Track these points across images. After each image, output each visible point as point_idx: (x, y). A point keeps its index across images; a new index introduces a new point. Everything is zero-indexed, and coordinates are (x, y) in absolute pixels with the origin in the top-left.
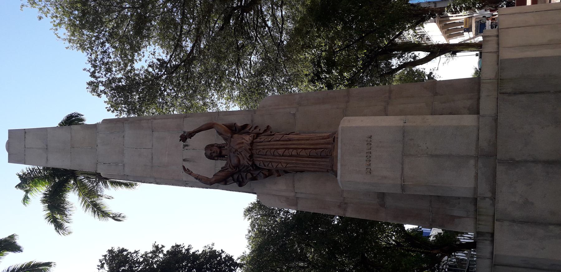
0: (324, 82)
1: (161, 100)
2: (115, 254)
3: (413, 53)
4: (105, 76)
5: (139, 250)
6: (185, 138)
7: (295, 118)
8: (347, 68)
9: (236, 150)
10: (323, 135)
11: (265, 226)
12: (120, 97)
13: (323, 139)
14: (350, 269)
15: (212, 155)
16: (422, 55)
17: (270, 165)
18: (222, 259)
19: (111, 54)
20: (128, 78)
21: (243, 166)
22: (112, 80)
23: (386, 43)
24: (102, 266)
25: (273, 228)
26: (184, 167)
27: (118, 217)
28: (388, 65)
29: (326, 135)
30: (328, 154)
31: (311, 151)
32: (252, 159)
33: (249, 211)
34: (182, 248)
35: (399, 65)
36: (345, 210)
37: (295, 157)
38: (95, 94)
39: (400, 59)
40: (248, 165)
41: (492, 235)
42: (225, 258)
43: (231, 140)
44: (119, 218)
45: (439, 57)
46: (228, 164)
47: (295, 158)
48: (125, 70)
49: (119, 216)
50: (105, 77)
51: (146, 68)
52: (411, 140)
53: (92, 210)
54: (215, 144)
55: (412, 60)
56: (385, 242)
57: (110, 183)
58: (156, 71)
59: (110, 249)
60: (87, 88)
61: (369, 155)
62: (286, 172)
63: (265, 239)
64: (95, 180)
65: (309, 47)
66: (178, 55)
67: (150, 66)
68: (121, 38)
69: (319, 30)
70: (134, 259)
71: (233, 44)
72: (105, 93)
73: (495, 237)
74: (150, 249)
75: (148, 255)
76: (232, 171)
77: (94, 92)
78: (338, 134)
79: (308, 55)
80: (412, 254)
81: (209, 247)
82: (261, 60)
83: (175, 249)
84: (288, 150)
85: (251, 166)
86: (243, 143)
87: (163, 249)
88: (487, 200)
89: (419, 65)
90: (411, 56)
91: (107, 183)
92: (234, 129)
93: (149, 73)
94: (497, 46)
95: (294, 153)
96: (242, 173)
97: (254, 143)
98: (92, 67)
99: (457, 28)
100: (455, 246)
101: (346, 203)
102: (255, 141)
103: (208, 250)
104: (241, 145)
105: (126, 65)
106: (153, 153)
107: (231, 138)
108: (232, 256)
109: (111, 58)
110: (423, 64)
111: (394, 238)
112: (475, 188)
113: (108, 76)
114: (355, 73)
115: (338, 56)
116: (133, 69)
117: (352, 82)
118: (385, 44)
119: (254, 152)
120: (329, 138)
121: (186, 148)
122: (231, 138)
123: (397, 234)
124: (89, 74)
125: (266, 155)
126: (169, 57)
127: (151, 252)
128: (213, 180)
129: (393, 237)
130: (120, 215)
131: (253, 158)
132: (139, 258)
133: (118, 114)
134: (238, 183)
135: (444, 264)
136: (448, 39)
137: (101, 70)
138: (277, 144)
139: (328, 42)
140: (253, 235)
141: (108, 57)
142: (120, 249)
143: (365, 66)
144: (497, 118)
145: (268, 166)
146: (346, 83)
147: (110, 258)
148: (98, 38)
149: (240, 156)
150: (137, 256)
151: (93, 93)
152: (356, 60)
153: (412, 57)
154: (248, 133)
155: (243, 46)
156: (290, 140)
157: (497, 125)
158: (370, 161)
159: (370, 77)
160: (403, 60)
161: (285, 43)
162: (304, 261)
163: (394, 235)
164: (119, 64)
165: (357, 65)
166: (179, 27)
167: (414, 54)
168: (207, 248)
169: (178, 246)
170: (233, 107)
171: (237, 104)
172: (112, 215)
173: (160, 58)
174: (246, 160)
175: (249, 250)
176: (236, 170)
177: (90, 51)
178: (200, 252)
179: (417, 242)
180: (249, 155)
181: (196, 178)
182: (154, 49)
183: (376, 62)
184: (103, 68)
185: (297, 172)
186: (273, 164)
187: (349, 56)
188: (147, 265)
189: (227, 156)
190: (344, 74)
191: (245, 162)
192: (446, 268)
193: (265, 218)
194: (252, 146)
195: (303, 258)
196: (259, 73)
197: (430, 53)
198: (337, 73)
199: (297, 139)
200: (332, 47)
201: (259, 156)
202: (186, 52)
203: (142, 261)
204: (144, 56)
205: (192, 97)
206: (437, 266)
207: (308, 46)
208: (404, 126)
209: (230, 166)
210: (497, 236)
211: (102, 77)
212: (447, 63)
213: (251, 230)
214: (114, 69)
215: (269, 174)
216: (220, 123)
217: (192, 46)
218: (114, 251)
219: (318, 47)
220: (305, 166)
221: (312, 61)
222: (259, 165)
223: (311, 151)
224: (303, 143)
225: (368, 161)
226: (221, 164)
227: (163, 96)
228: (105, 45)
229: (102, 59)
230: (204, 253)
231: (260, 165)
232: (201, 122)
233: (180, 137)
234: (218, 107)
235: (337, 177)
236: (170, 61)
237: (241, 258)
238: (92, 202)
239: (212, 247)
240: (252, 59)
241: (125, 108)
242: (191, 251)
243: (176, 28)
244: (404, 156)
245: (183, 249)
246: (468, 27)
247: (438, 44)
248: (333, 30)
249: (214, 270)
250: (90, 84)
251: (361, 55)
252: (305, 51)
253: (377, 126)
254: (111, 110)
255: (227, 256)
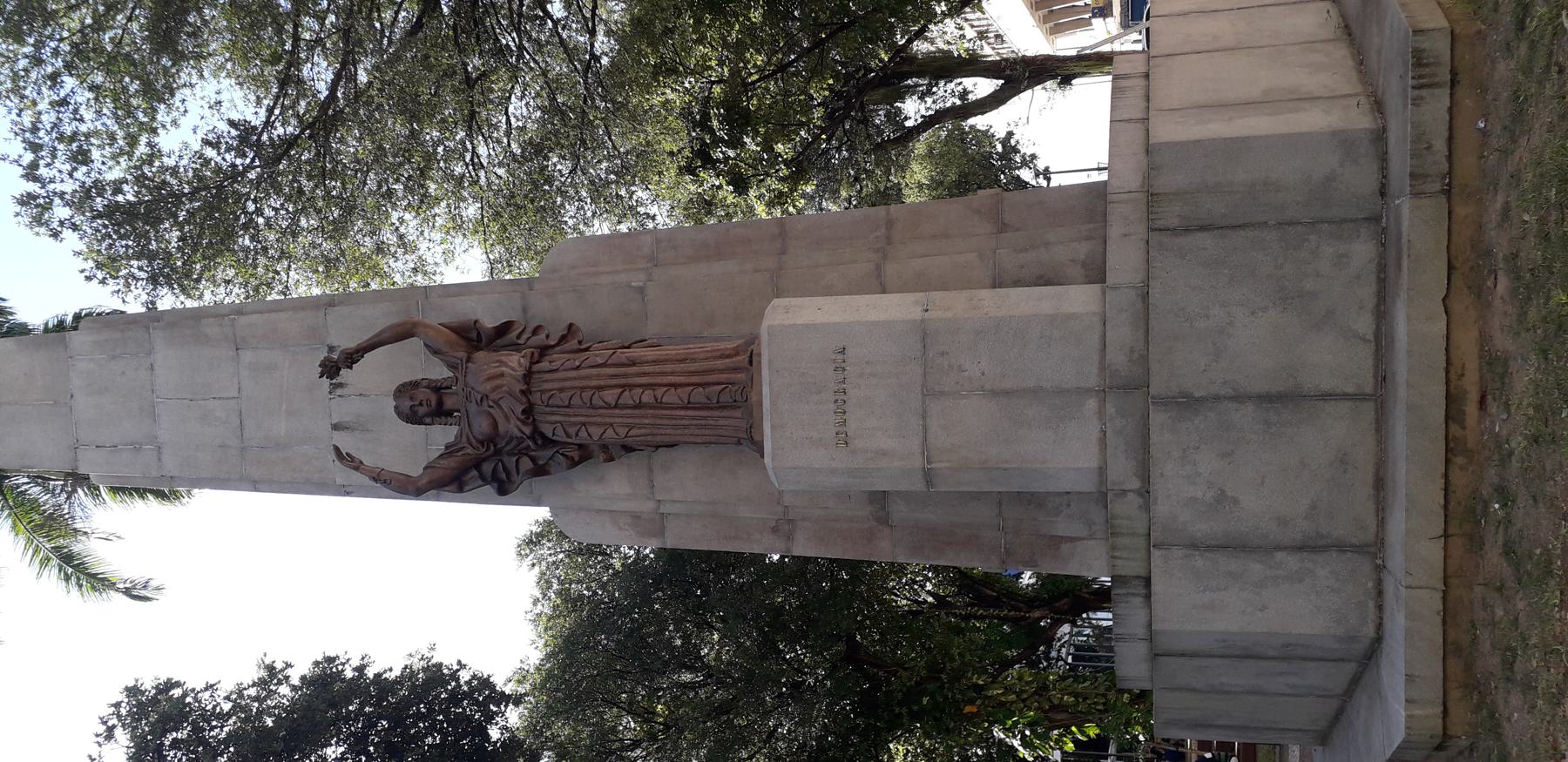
0: (722, 170)
1: (247, 242)
2: (147, 696)
3: (960, 83)
4: (71, 175)
5: (219, 682)
6: (334, 368)
7: (643, 300)
8: (784, 129)
9: (485, 397)
10: (723, 347)
11: (579, 582)
12: (121, 237)
13: (723, 356)
14: (816, 680)
15: (415, 413)
16: (982, 87)
17: (583, 434)
18: (461, 686)
19: (82, 111)
20: (140, 180)
21: (506, 440)
22: (91, 187)
23: (886, 59)
24: (110, 734)
25: (603, 586)
26: (337, 449)
27: (140, 589)
28: (895, 117)
29: (730, 345)
30: (738, 398)
31: (693, 390)
32: (532, 418)
33: (532, 542)
34: (343, 664)
35: (922, 116)
36: (790, 537)
37: (651, 408)
38: (43, 230)
39: (927, 99)
40: (522, 435)
41: (1147, 581)
42: (468, 683)
43: (466, 368)
44: (143, 593)
45: (1030, 91)
46: (464, 436)
47: (651, 411)
48: (130, 155)
49: (145, 587)
50: (71, 181)
51: (196, 146)
52: (942, 354)
53: (60, 571)
54: (423, 379)
55: (958, 102)
56: (908, 599)
57: (109, 490)
58: (227, 156)
59: (131, 684)
60: (17, 214)
61: (842, 398)
62: (628, 449)
63: (582, 620)
64: (62, 483)
65: (674, 71)
66: (293, 107)
67: (206, 142)
68: (112, 59)
69: (699, 21)
70: (204, 708)
71: (455, 73)
72: (75, 227)
73: (1152, 586)
74: (250, 674)
75: (245, 693)
76: (477, 454)
77: (40, 224)
78: (759, 345)
79: (671, 95)
80: (978, 625)
81: (420, 657)
82: (539, 114)
83: (324, 668)
84: (630, 390)
85: (528, 438)
86: (502, 375)
87: (289, 672)
88: (1131, 496)
89: (976, 115)
90: (953, 92)
91: (100, 492)
92: (474, 335)
93: (207, 162)
94: (1145, 104)
95: (647, 397)
96: (506, 459)
97: (533, 373)
98: (25, 149)
99: (1073, 6)
100: (1087, 596)
101: (790, 521)
102: (536, 367)
103: (418, 665)
104: (498, 382)
105: (133, 141)
106: (243, 411)
107: (468, 361)
108: (489, 676)
109: (83, 122)
110: (987, 112)
111: (929, 587)
112: (1101, 468)
113: (79, 175)
114: (806, 145)
115: (757, 95)
116: (155, 153)
117: (799, 169)
118: (881, 60)
119: (536, 398)
120: (737, 354)
121: (339, 392)
122: (468, 361)
123: (937, 576)
124: (20, 171)
125: (568, 406)
126: (263, 113)
127: (254, 685)
128: (424, 481)
129: (928, 584)
130: (147, 582)
131: (533, 416)
132: (219, 704)
133: (119, 287)
134: (496, 485)
135: (1062, 646)
136: (1053, 36)
137: (56, 158)
138: (598, 375)
139: (727, 56)
140: (546, 611)
141: (76, 119)
142: (161, 681)
143: (833, 119)
144: (1148, 292)
145: (577, 435)
146: (784, 172)
147: (131, 709)
148: (37, 61)
149: (495, 412)
150: (214, 697)
151: (37, 229)
152: (807, 108)
153: (957, 94)
154: (515, 347)
155: (484, 75)
156: (634, 364)
157: (1148, 309)
158: (845, 412)
159: (846, 151)
160: (934, 102)
161: (605, 61)
162: (691, 669)
163: (929, 579)
164: (112, 137)
165: (810, 120)
166: (289, 27)
167: (961, 87)
168: (416, 660)
169: (330, 660)
170: (465, 251)
171: (476, 243)
172: (121, 586)
173: (235, 116)
174: (514, 421)
175: (538, 652)
176: (486, 451)
177: (17, 101)
178: (397, 672)
179: (989, 592)
180: (523, 407)
181: (374, 478)
182: (218, 93)
183: (862, 108)
184: (60, 153)
185: (658, 447)
186: (592, 429)
187: (786, 93)
188: (246, 720)
189: (459, 411)
190: (775, 146)
191: (512, 427)
192: (1068, 654)
193: (580, 560)
194: (528, 383)
195: (688, 658)
196: (537, 149)
197: (1003, 82)
198: (757, 145)
199: (655, 358)
200: (739, 71)
201: (551, 409)
202: (314, 96)
203: (230, 710)
204: (186, 111)
205: (338, 230)
206: (1044, 652)
207: (669, 70)
208: (923, 321)
209: (468, 440)
210: (1157, 586)
211: (62, 181)
212: (1048, 108)
213: (540, 596)
214: (96, 154)
215: (582, 455)
216: (433, 319)
217: (332, 80)
218: (143, 688)
219: (701, 69)
220: (679, 432)
221: (686, 113)
222: (551, 435)
223: (693, 390)
224: (669, 370)
225: (841, 412)
226: (442, 435)
227: (254, 229)
228: (62, 82)
229: (55, 125)
230: (409, 674)
231: (554, 435)
232: (380, 319)
233: (320, 366)
234: (421, 252)
235: (762, 456)
236: (268, 124)
237: (516, 678)
238: (56, 549)
239: (430, 656)
240: (511, 109)
241: (140, 269)
242: (370, 673)
243: (279, 30)
244: (927, 397)
245: (346, 666)
246: (1101, 5)
247: (1024, 56)
248: (738, 20)
249: (441, 717)
250: (26, 200)
251: (819, 94)
252: (664, 83)
253: (858, 321)
254: (95, 276)
255: (474, 677)
